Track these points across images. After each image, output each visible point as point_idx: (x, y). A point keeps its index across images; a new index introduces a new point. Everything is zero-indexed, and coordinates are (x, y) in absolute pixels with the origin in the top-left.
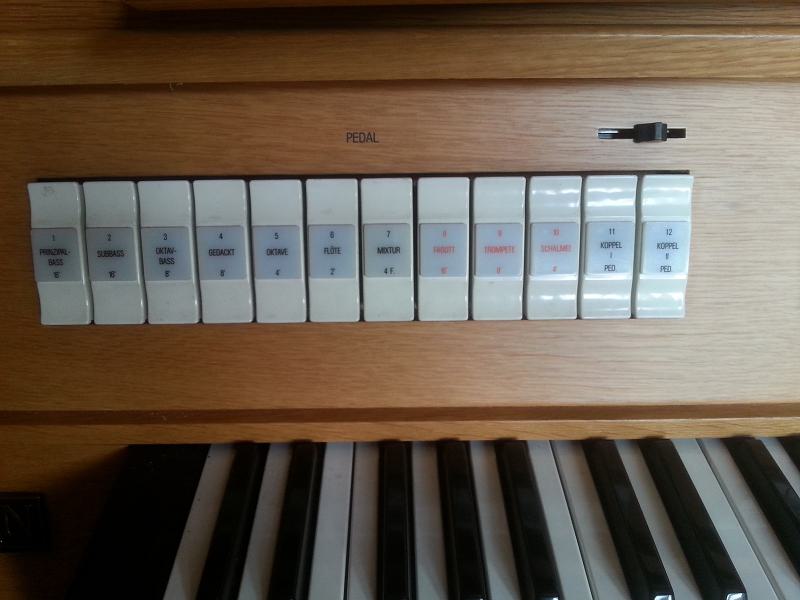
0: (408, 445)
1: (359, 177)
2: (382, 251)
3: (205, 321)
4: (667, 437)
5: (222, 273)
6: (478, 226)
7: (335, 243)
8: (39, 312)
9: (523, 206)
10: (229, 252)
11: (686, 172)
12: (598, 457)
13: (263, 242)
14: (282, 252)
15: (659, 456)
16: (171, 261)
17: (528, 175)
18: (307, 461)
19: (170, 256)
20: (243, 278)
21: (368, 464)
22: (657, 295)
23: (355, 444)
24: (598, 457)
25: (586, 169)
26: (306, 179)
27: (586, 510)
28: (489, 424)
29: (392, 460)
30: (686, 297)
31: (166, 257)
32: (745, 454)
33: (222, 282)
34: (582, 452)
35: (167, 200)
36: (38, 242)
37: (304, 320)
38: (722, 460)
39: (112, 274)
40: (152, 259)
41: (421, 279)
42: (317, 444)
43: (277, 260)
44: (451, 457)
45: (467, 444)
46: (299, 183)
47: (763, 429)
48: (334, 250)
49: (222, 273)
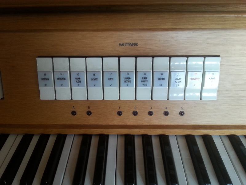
0: (134, 136)
1: (136, 57)
2: (43, 79)
3: (57, 99)
4: (210, 135)
5: (62, 85)
6: (138, 72)
7: (111, 77)
8: (39, 97)
9: (85, 67)
10: (48, 79)
11: (219, 56)
12: (190, 140)
13: (74, 76)
14: (96, 79)
15: (208, 140)
16: (80, 82)
17: (170, 57)
18: (103, 140)
19: (143, 80)
20: (116, 87)
21: (122, 141)
22: (191, 94)
23: (117, 135)
24: (190, 140)
25: (121, 55)
26: (154, 57)
27: (186, 154)
28: (76, 130)
29: (129, 140)
30: (217, 95)
31: (78, 80)
32: (234, 141)
33: (46, 88)
34: (185, 138)
35: (78, 63)
36: (40, 76)
37: (87, 99)
38: (227, 142)
39: (46, 85)
40: (74, 80)
41: (137, 87)
42: (133, 135)
43: (94, 82)
44: (146, 140)
45: (151, 136)
46: (101, 58)
47: (238, 133)
48: (112, 79)
49: (62, 85)
